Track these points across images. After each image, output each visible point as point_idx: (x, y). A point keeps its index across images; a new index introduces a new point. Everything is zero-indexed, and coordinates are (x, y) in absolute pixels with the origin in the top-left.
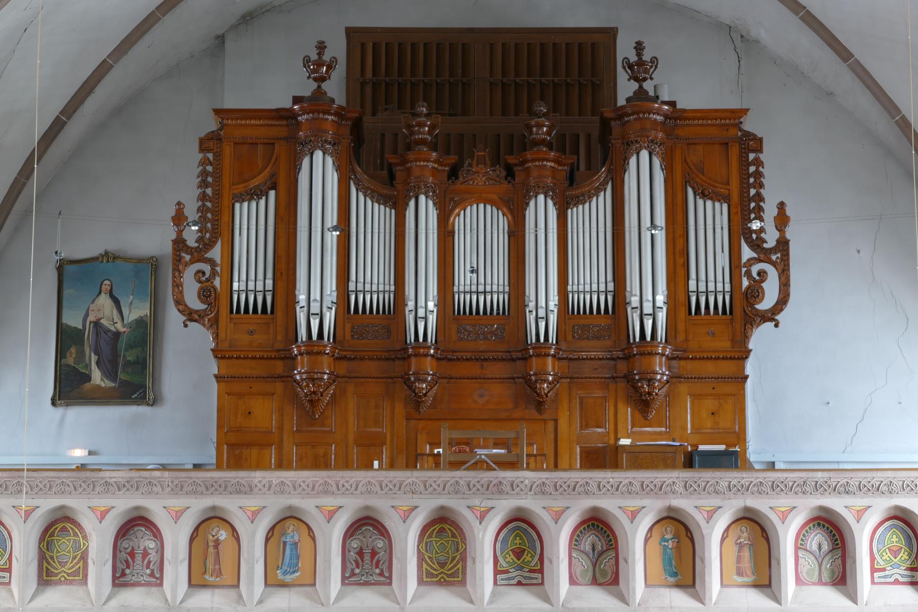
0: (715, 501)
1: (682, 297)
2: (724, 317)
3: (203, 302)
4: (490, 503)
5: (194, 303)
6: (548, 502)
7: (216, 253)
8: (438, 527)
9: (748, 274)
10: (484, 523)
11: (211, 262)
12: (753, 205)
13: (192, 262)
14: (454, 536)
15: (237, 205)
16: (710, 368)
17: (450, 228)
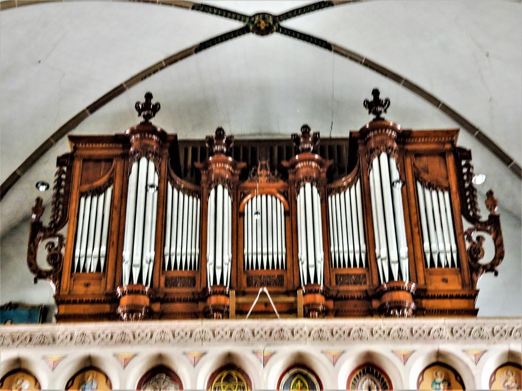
0: (481, 346)
1: (419, 254)
2: (453, 269)
3: (50, 264)
4: (272, 349)
5: (44, 265)
6: (326, 347)
7: (63, 231)
8: (225, 374)
9: (470, 239)
10: (267, 366)
11: (61, 238)
12: (468, 193)
13: (44, 238)
14: (239, 380)
15: (83, 200)
16: (447, 304)
17: (241, 209)
